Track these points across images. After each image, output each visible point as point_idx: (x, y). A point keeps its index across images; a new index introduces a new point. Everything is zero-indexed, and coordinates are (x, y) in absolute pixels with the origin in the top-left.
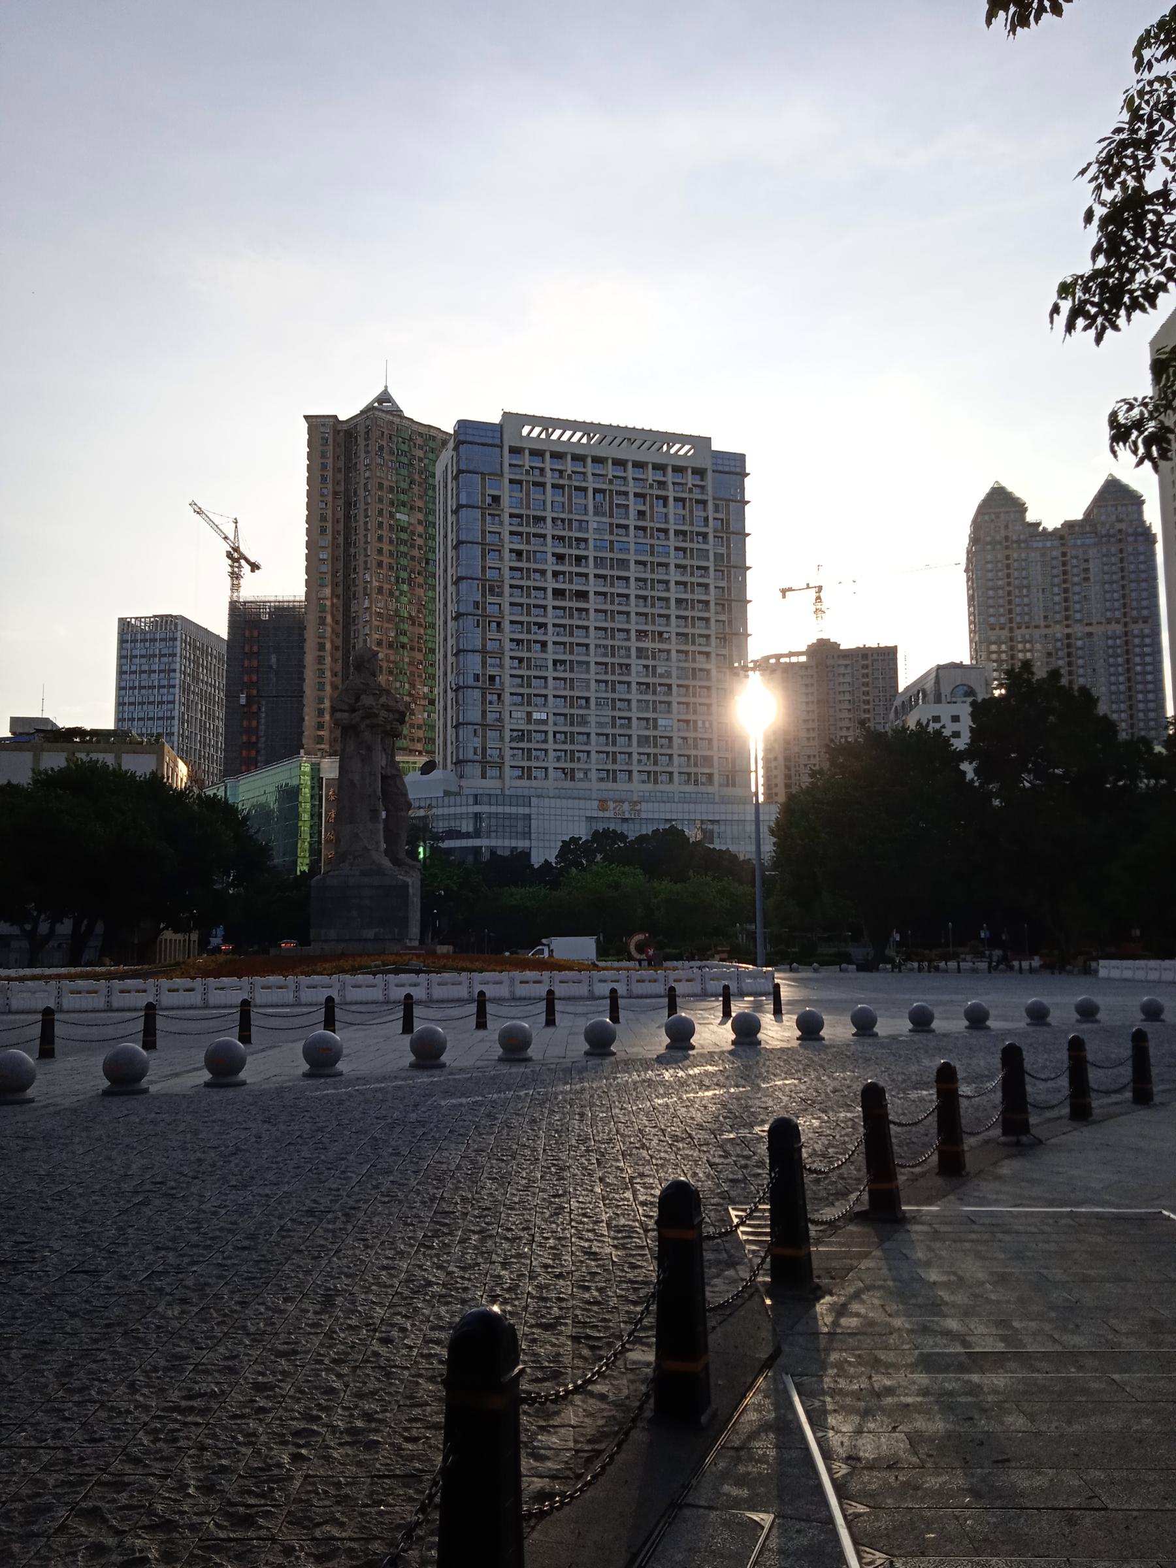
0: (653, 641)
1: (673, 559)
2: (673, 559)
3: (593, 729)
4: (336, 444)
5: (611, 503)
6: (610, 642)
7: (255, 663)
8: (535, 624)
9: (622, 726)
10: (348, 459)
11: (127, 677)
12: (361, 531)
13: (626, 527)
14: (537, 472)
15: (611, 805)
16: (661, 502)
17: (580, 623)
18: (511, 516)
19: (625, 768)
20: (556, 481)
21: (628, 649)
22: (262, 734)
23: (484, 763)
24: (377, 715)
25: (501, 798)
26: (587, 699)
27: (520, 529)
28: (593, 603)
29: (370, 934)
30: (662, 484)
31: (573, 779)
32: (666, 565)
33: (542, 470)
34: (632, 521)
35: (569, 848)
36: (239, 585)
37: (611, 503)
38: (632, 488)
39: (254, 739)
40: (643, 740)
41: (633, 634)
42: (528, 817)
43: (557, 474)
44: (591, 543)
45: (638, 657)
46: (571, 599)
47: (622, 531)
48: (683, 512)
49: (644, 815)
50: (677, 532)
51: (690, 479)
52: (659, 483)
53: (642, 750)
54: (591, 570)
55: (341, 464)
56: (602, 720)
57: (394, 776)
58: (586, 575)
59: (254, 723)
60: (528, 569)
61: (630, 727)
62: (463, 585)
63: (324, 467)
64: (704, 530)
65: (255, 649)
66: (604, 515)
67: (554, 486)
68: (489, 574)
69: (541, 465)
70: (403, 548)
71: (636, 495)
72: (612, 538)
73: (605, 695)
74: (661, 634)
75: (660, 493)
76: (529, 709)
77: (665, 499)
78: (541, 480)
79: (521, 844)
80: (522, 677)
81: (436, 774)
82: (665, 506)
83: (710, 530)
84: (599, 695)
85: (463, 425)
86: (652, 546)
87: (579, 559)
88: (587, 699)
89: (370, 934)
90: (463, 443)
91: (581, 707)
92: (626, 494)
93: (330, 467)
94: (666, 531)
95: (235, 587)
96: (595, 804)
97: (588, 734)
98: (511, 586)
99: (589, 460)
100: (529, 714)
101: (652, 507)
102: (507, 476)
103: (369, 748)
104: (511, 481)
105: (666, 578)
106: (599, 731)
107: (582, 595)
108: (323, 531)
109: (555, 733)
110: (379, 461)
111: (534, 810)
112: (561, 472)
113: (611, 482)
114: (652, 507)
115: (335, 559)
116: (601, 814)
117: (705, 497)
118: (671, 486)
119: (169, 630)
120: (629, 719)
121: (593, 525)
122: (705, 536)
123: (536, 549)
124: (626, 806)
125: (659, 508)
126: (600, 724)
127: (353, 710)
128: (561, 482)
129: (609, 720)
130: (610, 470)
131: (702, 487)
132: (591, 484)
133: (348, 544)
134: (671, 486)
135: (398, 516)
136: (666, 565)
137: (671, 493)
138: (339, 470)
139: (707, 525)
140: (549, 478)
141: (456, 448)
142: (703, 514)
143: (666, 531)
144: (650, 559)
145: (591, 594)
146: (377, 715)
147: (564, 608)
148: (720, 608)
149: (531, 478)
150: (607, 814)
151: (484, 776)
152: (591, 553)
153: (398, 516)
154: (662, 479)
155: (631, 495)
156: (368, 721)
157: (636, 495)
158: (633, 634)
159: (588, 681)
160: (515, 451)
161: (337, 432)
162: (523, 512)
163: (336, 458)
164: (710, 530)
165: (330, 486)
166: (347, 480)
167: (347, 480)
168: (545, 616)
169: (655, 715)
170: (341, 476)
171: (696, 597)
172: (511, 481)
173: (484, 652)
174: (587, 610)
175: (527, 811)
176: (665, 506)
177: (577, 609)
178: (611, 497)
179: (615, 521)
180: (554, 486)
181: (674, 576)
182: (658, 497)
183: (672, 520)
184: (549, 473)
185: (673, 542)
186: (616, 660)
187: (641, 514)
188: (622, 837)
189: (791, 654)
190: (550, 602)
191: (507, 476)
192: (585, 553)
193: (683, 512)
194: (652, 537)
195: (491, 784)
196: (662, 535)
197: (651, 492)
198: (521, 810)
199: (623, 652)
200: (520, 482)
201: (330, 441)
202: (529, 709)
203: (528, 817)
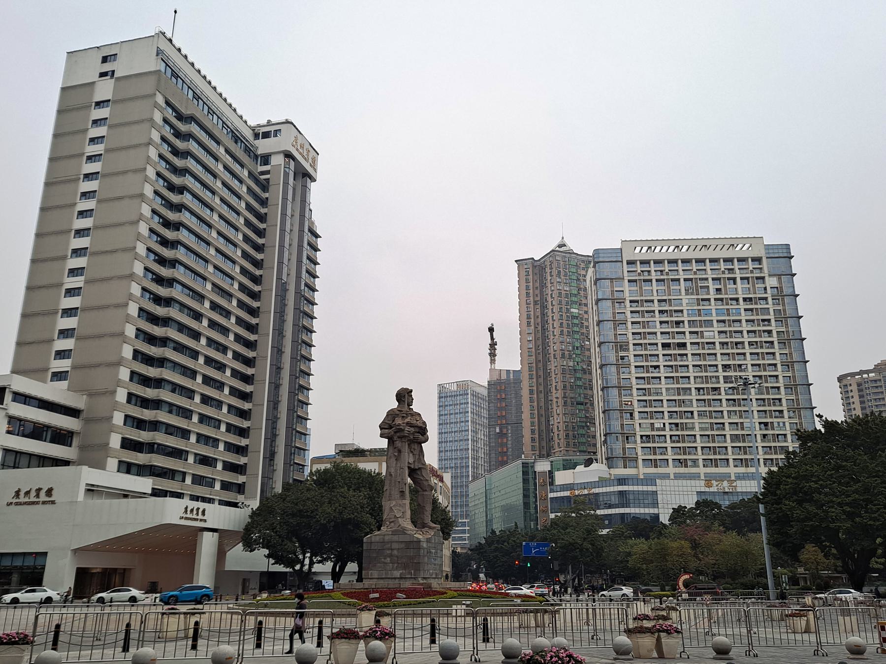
0: (735, 371)
1: (744, 317)
2: (744, 317)
3: (697, 432)
4: (534, 274)
5: (697, 287)
6: (704, 374)
7: (504, 404)
8: (651, 366)
9: (718, 429)
10: (541, 282)
11: (442, 418)
12: (550, 321)
13: (709, 300)
14: (646, 274)
15: (714, 483)
16: (732, 281)
17: (682, 363)
18: (631, 301)
19: (723, 457)
20: (658, 278)
21: (717, 377)
22: (510, 446)
23: (625, 459)
24: (403, 430)
25: (635, 480)
26: (692, 413)
27: (638, 309)
28: (689, 350)
29: (397, 574)
30: (731, 270)
31: (686, 466)
32: (740, 321)
33: (649, 271)
34: (712, 295)
35: (679, 513)
36: (494, 360)
37: (697, 287)
38: (710, 275)
39: (505, 450)
40: (735, 438)
41: (720, 367)
42: (655, 493)
43: (659, 273)
44: (685, 312)
45: (725, 382)
46: (674, 349)
47: (707, 303)
48: (748, 286)
49: (739, 490)
50: (745, 299)
51: (751, 265)
52: (729, 269)
53: (734, 445)
54: (687, 329)
55: (538, 285)
56: (703, 426)
57: (420, 469)
58: (684, 333)
59: (505, 440)
60: (730, 331)
61: (724, 430)
62: (603, 346)
63: (527, 288)
64: (765, 295)
65: (503, 396)
66: (692, 294)
67: (657, 280)
68: (619, 339)
69: (648, 269)
70: (576, 329)
71: (713, 279)
72: (699, 308)
73: (704, 409)
74: (740, 366)
75: (730, 276)
76: (652, 421)
77: (734, 279)
78: (649, 278)
79: (655, 511)
80: (646, 401)
81: (594, 466)
82: (735, 283)
83: (769, 295)
84: (700, 409)
85: (596, 251)
86: (728, 310)
87: (678, 323)
88: (692, 413)
89: (397, 574)
90: (598, 262)
91: (687, 418)
92: (707, 279)
93: (531, 287)
94: (737, 300)
95: (493, 361)
96: (703, 483)
97: (695, 436)
98: (634, 345)
99: (736, 260)
100: (652, 424)
101: (725, 286)
102: (626, 278)
103: (400, 451)
104: (629, 281)
105: (740, 329)
106: (702, 433)
107: (683, 345)
108: (529, 324)
109: (671, 436)
110: (558, 280)
111: (659, 488)
112: (661, 271)
113: (695, 273)
114: (725, 286)
115: (536, 339)
116: (707, 490)
117: (762, 275)
118: (738, 271)
119: (464, 389)
120: (723, 424)
121: (685, 302)
122: (766, 299)
123: (649, 319)
124: (725, 484)
125: (731, 286)
126: (701, 429)
127: (391, 427)
128: (662, 277)
129: (649, 426)
130: (694, 266)
131: (761, 269)
132: (682, 276)
133: (544, 330)
134: (738, 271)
135: (572, 310)
136: (740, 321)
137: (738, 275)
138: (537, 288)
139: (766, 293)
140: (654, 276)
141: (594, 267)
142: (763, 286)
143: (737, 300)
144: (727, 318)
145: (688, 345)
146: (403, 430)
147: (670, 355)
148: (782, 346)
149: (642, 278)
150: (712, 490)
151: (625, 467)
152: (686, 319)
153: (572, 310)
154: (731, 267)
155: (710, 280)
156: (398, 434)
157: (713, 279)
158: (720, 367)
159: (691, 401)
160: (630, 263)
161: (534, 267)
162: (638, 298)
163: (534, 281)
164: (769, 295)
165: (532, 298)
166: (541, 292)
167: (541, 292)
168: (658, 361)
169: (741, 421)
170: (537, 292)
171: (764, 339)
172: (629, 281)
173: (619, 388)
174: (686, 355)
175: (654, 488)
176: (735, 283)
177: (679, 355)
178: (696, 283)
179: (700, 297)
180: (657, 280)
181: (745, 327)
182: (729, 279)
183: (740, 292)
184: (653, 273)
185: (742, 305)
186: (710, 386)
187: (718, 290)
188: (719, 506)
189: (861, 372)
190: (660, 351)
191: (626, 278)
192: (682, 319)
193: (748, 286)
194: (727, 304)
195: (629, 472)
196: (734, 302)
197: (723, 276)
198: (650, 488)
199: (714, 380)
200: (747, 278)
201: (531, 273)
202: (652, 421)
203: (655, 493)
